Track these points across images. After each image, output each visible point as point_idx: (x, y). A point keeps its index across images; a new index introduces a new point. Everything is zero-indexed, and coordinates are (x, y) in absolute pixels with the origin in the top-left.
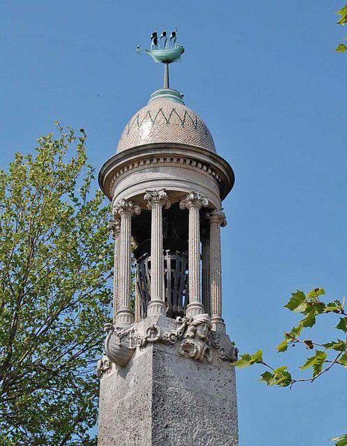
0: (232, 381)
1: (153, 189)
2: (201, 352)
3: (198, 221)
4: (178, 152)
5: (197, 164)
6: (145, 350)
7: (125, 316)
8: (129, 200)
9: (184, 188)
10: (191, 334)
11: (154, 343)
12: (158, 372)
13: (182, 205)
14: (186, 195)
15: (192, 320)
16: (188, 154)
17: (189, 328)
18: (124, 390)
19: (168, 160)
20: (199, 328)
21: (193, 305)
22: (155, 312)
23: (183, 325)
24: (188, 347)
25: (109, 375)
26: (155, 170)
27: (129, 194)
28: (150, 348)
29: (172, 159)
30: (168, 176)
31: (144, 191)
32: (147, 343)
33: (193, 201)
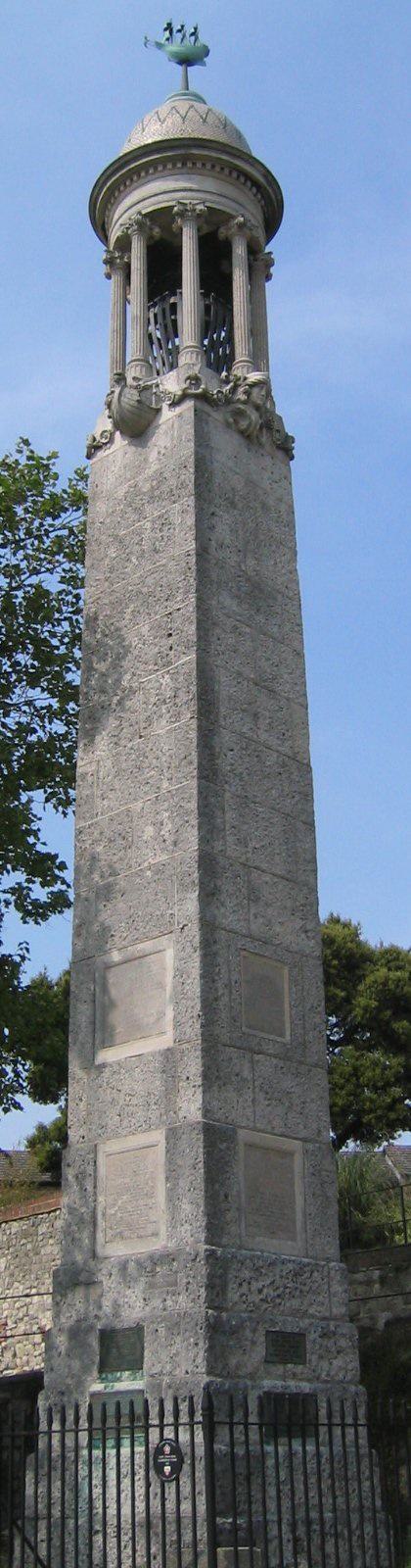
0: (287, 478)
1: (187, 202)
2: (256, 425)
3: (146, 278)
4: (214, 154)
5: (238, 177)
6: (178, 410)
7: (187, 352)
8: (146, 215)
9: (218, 203)
10: (243, 397)
11: (196, 397)
12: (201, 439)
13: (222, 233)
14: (233, 217)
15: (245, 379)
16: (237, 162)
17: (241, 390)
18: (140, 468)
19: (209, 166)
20: (255, 391)
21: (241, 361)
22: (190, 359)
23: (232, 384)
24: (239, 414)
25: (108, 452)
26: (177, 180)
27: (148, 207)
28: (189, 404)
29: (213, 167)
30: (194, 186)
31: (174, 203)
32: (184, 397)
33: (241, 226)
